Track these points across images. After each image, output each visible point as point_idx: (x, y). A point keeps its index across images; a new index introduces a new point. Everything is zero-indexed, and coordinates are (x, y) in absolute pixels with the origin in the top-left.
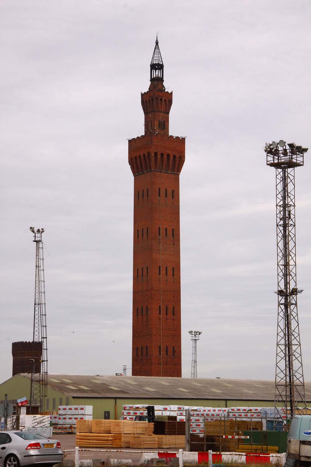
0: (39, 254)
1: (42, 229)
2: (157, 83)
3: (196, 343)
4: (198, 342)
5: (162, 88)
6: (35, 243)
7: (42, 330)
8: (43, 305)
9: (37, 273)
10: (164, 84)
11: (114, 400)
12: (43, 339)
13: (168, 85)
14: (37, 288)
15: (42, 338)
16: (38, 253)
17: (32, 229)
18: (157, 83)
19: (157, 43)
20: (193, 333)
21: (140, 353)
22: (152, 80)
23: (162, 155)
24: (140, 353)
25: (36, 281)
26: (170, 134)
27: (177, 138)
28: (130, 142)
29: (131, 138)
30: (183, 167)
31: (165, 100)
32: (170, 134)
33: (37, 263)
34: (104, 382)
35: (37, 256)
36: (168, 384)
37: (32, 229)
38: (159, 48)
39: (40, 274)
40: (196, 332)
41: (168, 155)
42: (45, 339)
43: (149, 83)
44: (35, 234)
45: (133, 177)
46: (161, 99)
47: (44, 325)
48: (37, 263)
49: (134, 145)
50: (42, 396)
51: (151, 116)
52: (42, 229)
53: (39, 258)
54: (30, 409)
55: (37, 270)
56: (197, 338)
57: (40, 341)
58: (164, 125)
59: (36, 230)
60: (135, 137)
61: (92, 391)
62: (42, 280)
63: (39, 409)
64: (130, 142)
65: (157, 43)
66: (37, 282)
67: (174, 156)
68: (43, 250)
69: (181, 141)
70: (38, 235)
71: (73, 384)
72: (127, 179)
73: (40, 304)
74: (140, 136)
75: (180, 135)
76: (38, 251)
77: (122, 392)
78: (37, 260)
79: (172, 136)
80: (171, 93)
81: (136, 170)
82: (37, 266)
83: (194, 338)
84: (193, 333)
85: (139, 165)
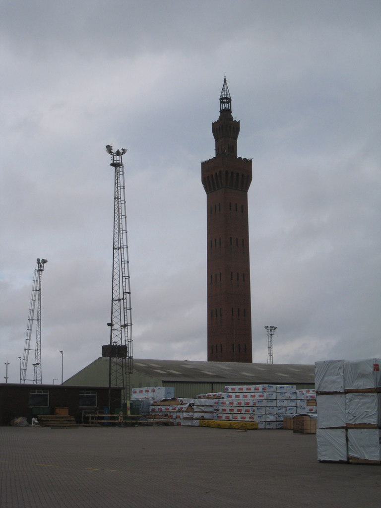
0: (119, 181)
1: (123, 149)
2: (226, 114)
3: (271, 337)
4: (273, 336)
5: (231, 118)
6: (113, 168)
7: (124, 283)
8: (125, 249)
9: (116, 207)
10: (232, 114)
11: (211, 385)
12: (125, 296)
13: (236, 115)
14: (116, 227)
15: (124, 293)
16: (117, 180)
17: (109, 148)
18: (226, 114)
19: (225, 81)
20: (269, 328)
21: (215, 350)
22: (221, 111)
23: (232, 173)
24: (215, 350)
25: (114, 218)
26: (239, 156)
27: (245, 159)
28: (203, 164)
29: (203, 161)
30: (159, 359)
31: (233, 127)
32: (239, 156)
33: (116, 193)
34: (195, 367)
35: (116, 186)
36: (264, 370)
37: (109, 148)
38: (226, 85)
39: (120, 207)
40: (271, 327)
41: (238, 174)
42: (128, 295)
43: (219, 114)
44: (113, 156)
45: (205, 195)
46: (230, 127)
47: (128, 291)
48: (116, 193)
49: (207, 167)
50: (126, 373)
51: (221, 141)
52: (123, 149)
53: (119, 185)
54: (109, 391)
55: (116, 203)
56: (272, 333)
57: (123, 344)
58: (233, 148)
59: (114, 150)
60: (207, 160)
61: (185, 376)
62: (128, 306)
63: (122, 391)
64: (203, 164)
65: (225, 81)
66: (116, 219)
67: (243, 175)
68: (123, 176)
69: (248, 163)
70: (117, 158)
71: (161, 369)
72: (200, 196)
73: (121, 248)
74: (211, 158)
75: (248, 157)
76: (118, 177)
77: (217, 376)
78: (116, 189)
79: (240, 158)
80: (239, 122)
81: (208, 188)
82: (117, 198)
83: (270, 333)
84: (269, 328)
85: (211, 182)
